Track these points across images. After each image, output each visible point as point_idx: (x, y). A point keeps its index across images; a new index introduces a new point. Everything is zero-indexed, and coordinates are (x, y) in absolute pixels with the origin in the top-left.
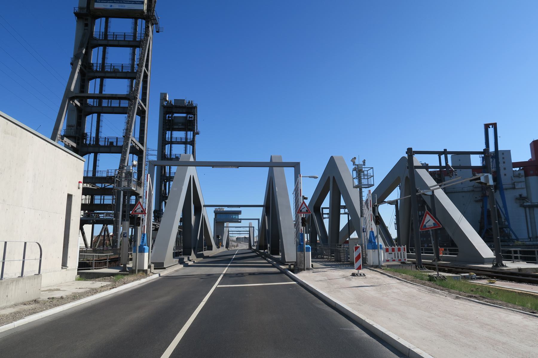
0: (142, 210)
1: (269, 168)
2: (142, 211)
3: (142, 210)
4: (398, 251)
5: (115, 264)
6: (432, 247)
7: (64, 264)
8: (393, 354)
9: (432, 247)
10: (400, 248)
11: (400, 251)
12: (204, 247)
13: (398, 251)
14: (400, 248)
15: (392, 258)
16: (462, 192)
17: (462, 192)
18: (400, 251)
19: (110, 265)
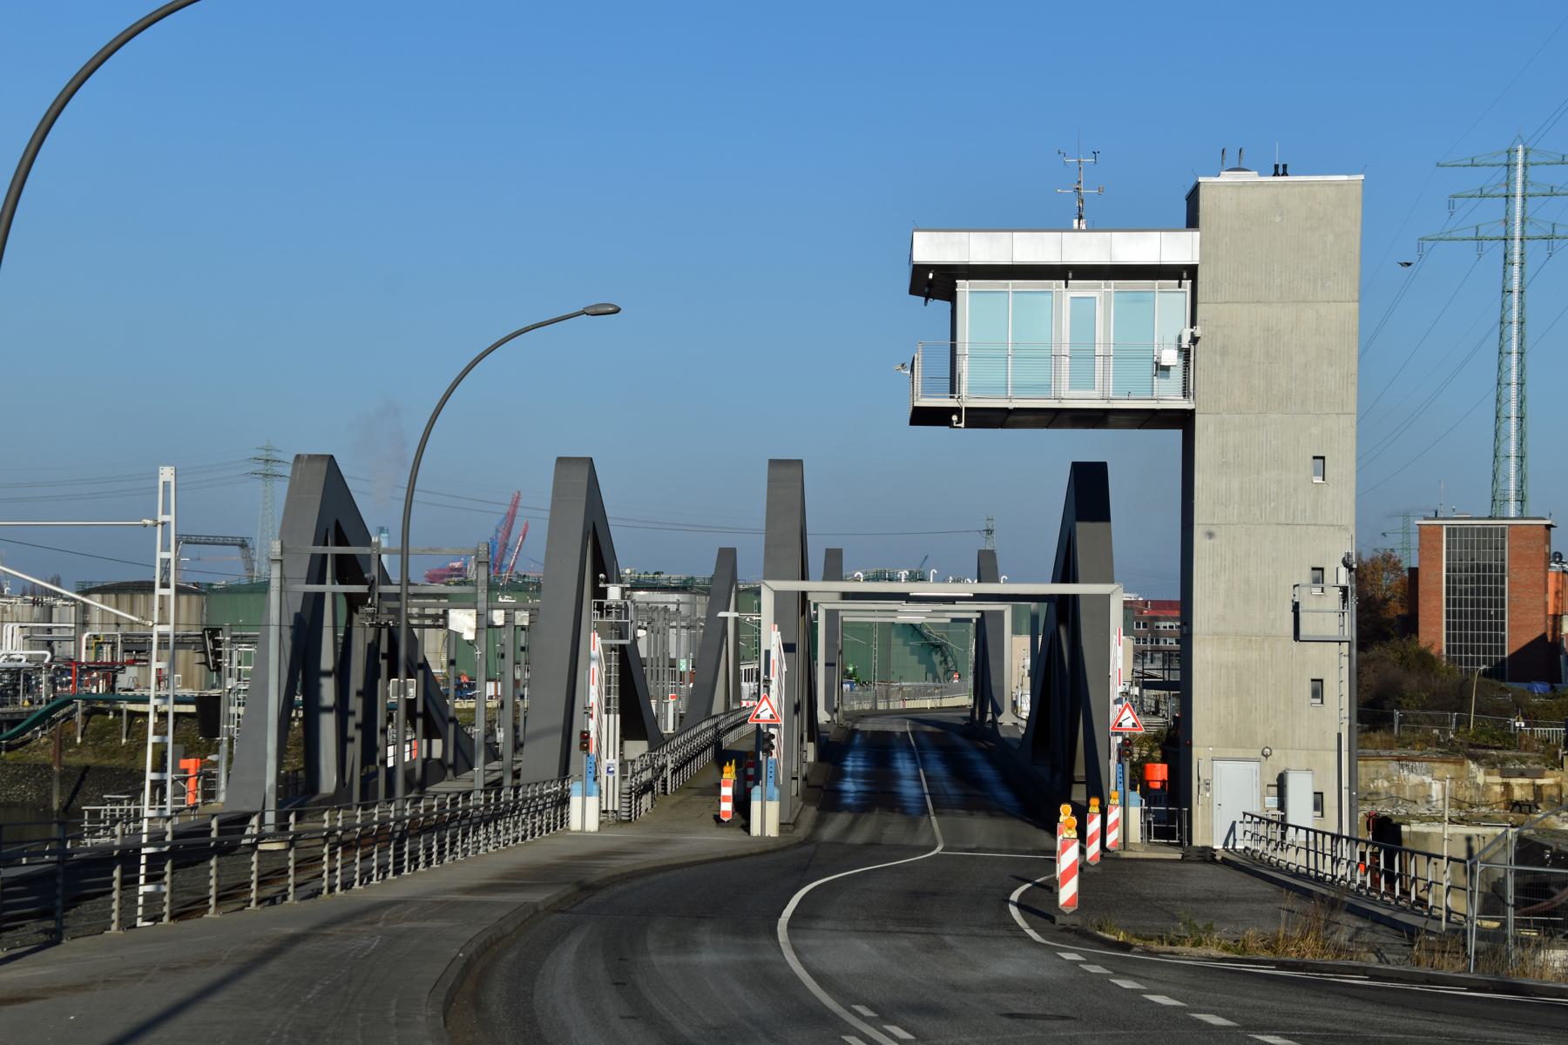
0: (1134, 721)
3: (1134, 721)
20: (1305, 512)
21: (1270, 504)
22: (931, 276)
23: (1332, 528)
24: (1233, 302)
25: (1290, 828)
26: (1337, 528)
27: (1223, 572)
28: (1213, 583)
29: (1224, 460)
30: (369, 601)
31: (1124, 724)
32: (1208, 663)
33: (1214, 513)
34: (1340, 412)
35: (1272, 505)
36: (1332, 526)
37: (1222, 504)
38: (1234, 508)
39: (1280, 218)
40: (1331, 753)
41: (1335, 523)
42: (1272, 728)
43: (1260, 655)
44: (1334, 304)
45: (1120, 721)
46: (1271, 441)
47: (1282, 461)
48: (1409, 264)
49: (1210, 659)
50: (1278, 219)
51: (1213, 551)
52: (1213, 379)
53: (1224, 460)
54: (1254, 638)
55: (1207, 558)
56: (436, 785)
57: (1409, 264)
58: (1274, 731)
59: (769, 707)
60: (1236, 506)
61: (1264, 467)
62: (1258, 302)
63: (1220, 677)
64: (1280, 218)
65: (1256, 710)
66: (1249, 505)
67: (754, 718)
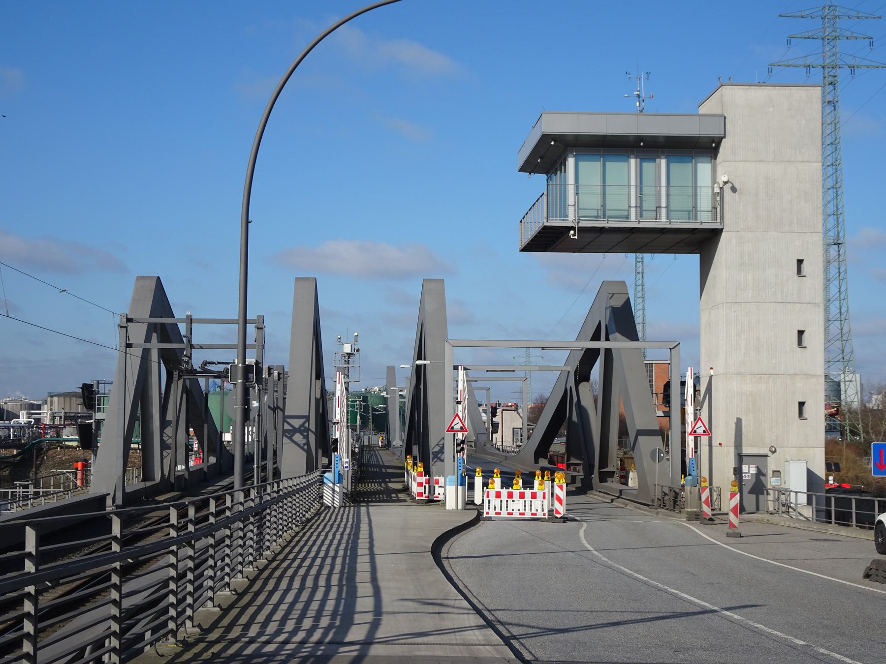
0: (705, 429)
1: (247, 350)
2: (704, 431)
3: (705, 429)
4: (508, 498)
5: (403, 434)
6: (607, 339)
7: (496, 438)
8: (452, 586)
9: (607, 339)
10: (524, 493)
11: (500, 498)
12: (97, 406)
13: (508, 498)
14: (524, 493)
15: (513, 501)
16: (816, 540)
17: (816, 540)
18: (500, 498)
19: (403, 434)
20: (793, 294)
21: (771, 289)
22: (642, 144)
23: (809, 305)
24: (745, 161)
25: (127, 491)
26: (813, 304)
27: (743, 333)
28: (737, 341)
29: (742, 261)
30: (185, 353)
31: (698, 431)
32: (734, 392)
33: (737, 296)
34: (813, 231)
35: (773, 290)
36: (810, 303)
37: (742, 290)
38: (749, 292)
39: (773, 109)
40: (731, 448)
41: (812, 302)
42: (775, 434)
43: (767, 387)
44: (807, 163)
45: (452, 425)
46: (771, 250)
47: (778, 262)
48: (5, 117)
49: (735, 390)
50: (771, 110)
51: (737, 320)
52: (734, 210)
53: (742, 261)
54: (763, 376)
55: (733, 324)
56: (231, 477)
57: (5, 117)
58: (776, 435)
59: (702, 425)
60: (750, 291)
61: (767, 266)
62: (761, 161)
63: (742, 401)
64: (773, 109)
65: (765, 422)
66: (759, 291)
67: (450, 430)
